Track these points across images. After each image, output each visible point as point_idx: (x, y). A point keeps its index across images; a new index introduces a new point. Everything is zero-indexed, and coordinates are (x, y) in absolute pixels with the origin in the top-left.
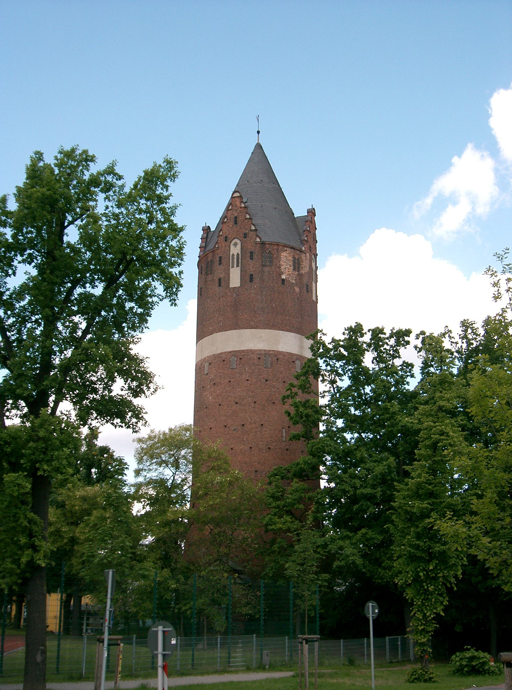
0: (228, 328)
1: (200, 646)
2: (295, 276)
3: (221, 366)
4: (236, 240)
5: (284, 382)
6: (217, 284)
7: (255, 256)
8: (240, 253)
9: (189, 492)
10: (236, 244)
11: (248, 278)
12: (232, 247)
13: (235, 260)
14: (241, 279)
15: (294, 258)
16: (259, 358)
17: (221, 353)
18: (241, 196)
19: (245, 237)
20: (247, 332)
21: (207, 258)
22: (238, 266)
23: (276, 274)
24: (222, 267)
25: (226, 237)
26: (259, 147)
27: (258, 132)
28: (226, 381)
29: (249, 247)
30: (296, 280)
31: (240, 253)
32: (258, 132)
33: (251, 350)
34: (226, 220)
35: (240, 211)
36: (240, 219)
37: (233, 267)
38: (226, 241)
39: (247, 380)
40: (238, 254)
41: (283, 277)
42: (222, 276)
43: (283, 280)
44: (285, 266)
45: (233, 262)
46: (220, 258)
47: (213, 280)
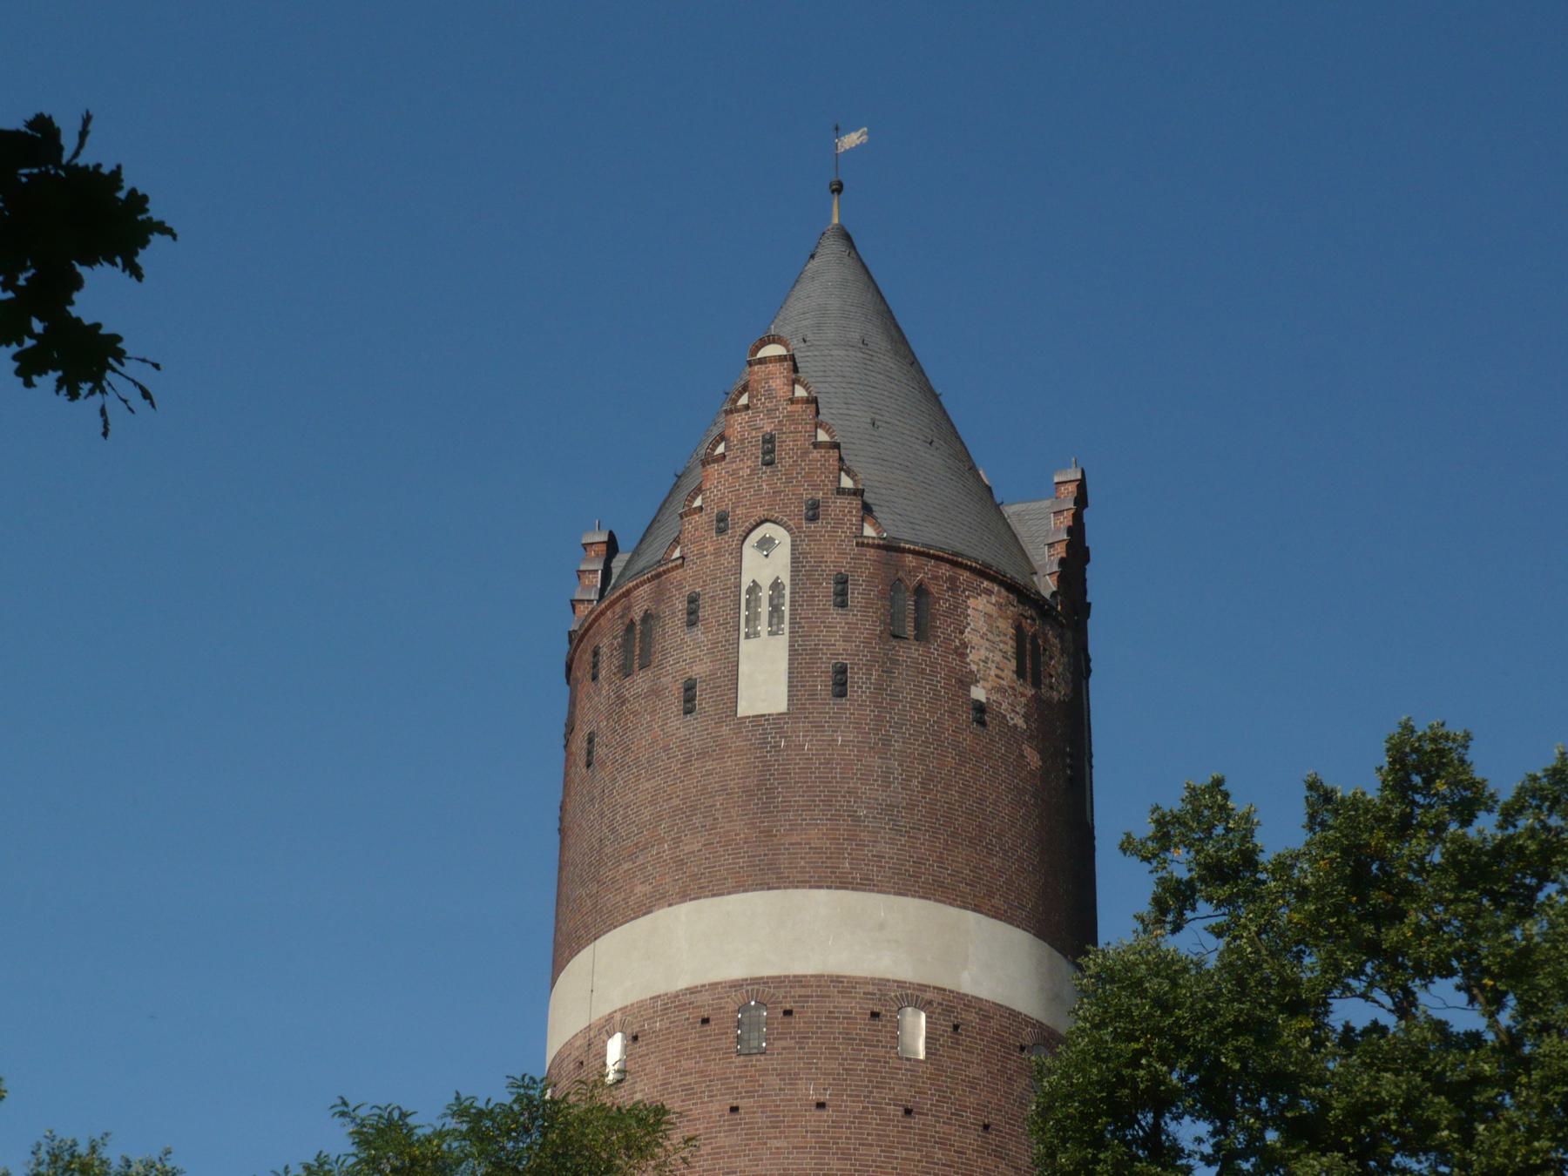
0: (730, 883)
2: (1023, 700)
3: (688, 1045)
4: (767, 529)
5: (986, 1127)
6: (676, 706)
7: (855, 596)
10: (766, 544)
11: (823, 685)
12: (749, 551)
13: (764, 609)
14: (791, 686)
15: (1019, 628)
16: (875, 1015)
17: (693, 991)
18: (792, 358)
19: (813, 518)
20: (820, 901)
21: (628, 608)
22: (755, 587)
23: (948, 677)
24: (699, 633)
25: (722, 518)
28: (718, 1106)
29: (829, 558)
30: (1026, 717)
31: (786, 579)
33: (836, 980)
34: (721, 449)
35: (790, 416)
36: (788, 445)
38: (721, 531)
39: (821, 1105)
40: (776, 586)
41: (978, 693)
42: (699, 670)
43: (980, 708)
44: (983, 653)
46: (693, 600)
47: (656, 692)
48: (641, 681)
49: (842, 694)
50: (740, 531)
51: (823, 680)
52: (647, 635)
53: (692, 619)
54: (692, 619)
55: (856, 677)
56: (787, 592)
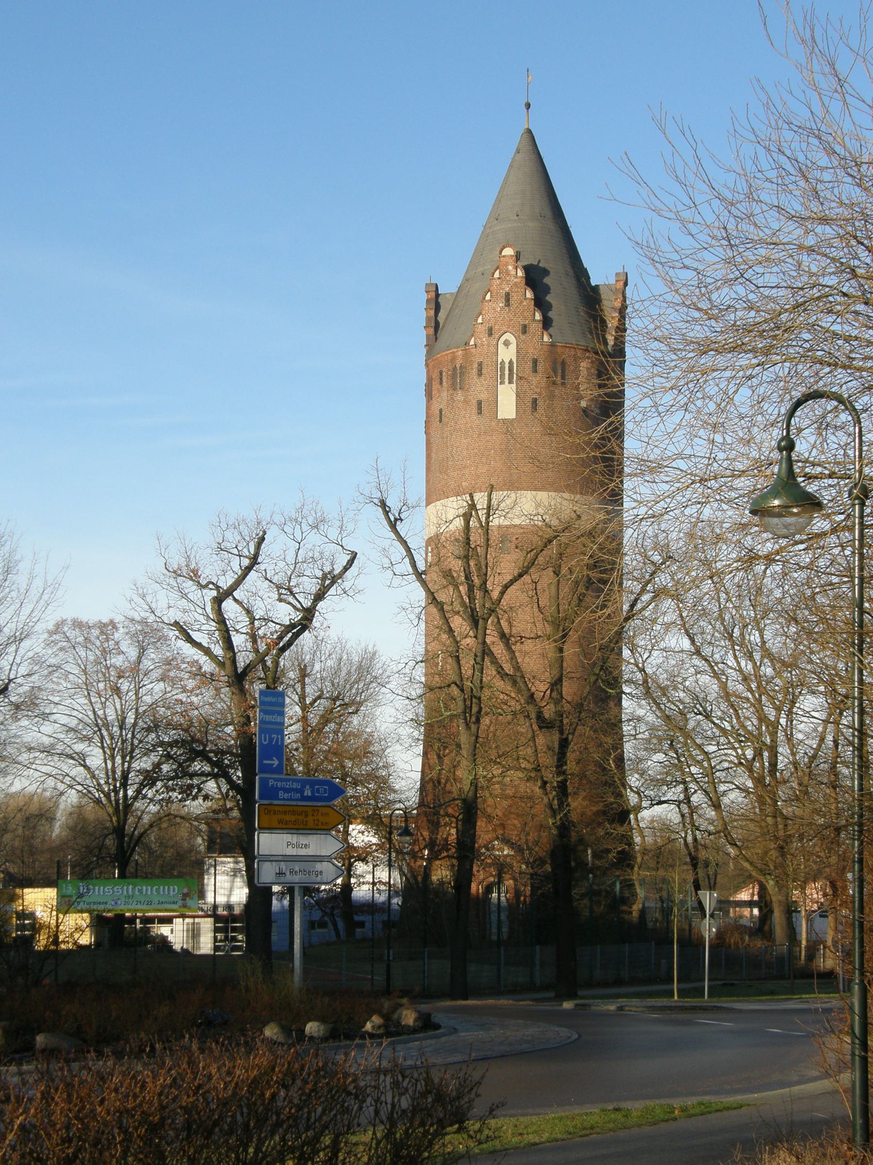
1: (72, 797)
6: (475, 410)
7: (540, 368)
8: (514, 360)
9: (638, 891)
10: (507, 343)
13: (507, 372)
22: (510, 382)
26: (529, 131)
27: (528, 106)
31: (514, 360)
32: (528, 106)
37: (502, 383)
40: (511, 362)
42: (483, 396)
45: (503, 375)
46: (480, 365)
47: (466, 401)
48: (460, 396)
49: (508, 305)
50: (497, 336)
51: (529, 405)
52: (462, 374)
53: (480, 373)
54: (480, 373)
55: (540, 403)
56: (515, 365)
